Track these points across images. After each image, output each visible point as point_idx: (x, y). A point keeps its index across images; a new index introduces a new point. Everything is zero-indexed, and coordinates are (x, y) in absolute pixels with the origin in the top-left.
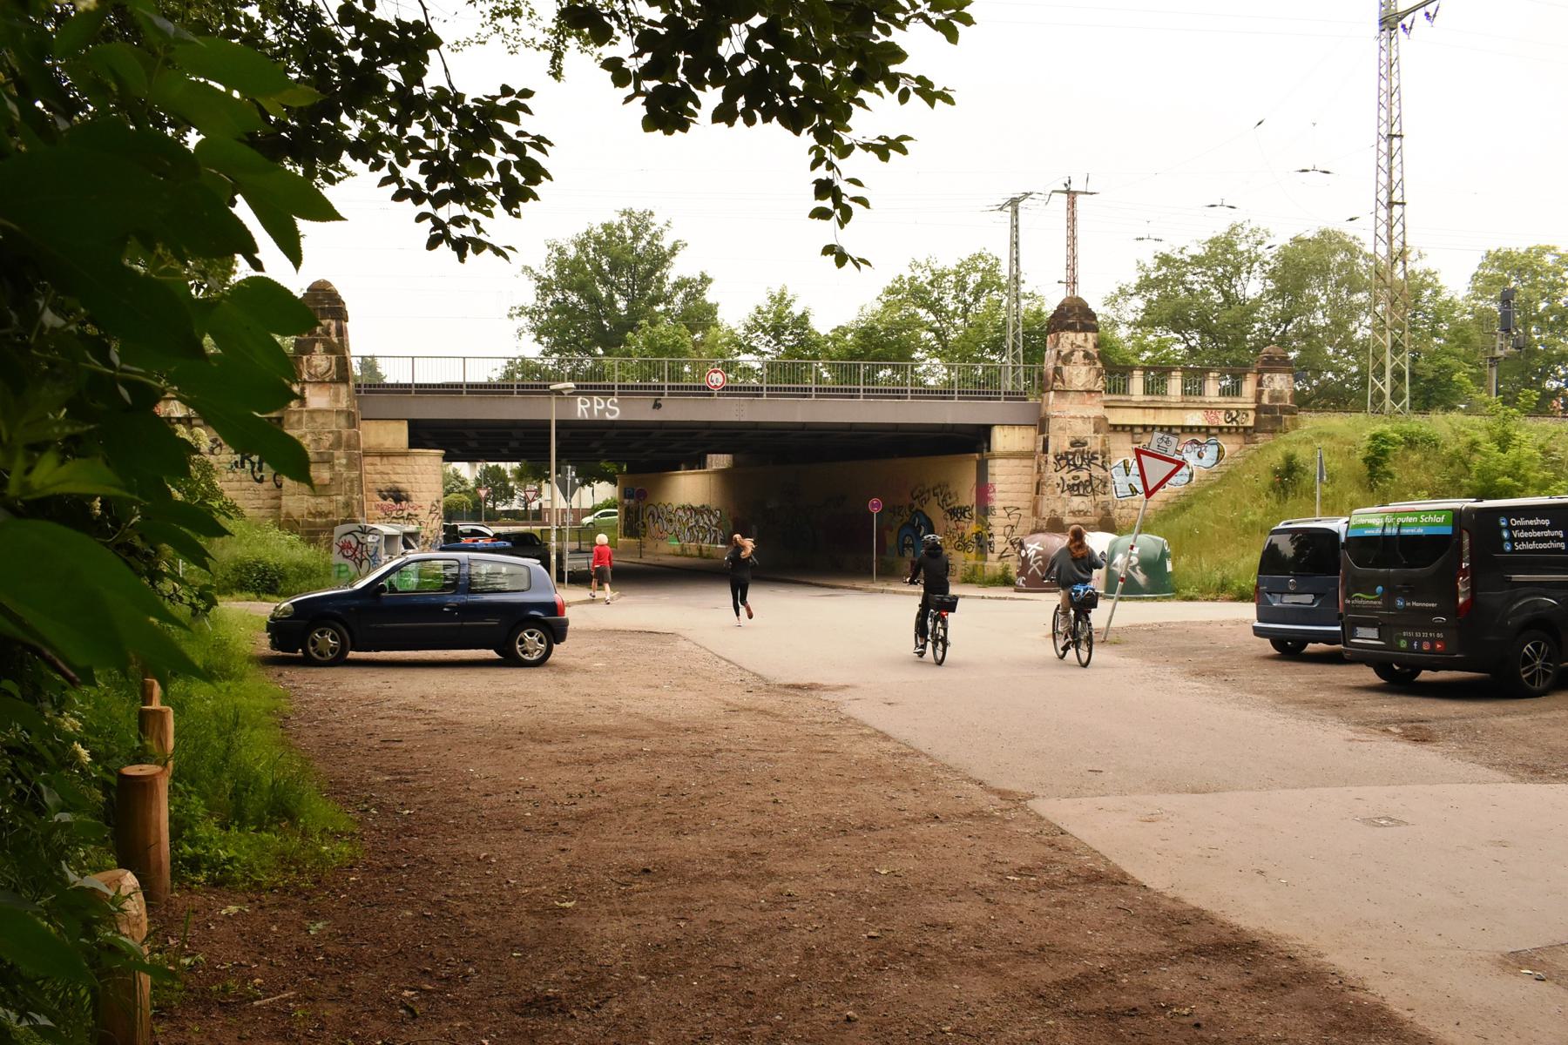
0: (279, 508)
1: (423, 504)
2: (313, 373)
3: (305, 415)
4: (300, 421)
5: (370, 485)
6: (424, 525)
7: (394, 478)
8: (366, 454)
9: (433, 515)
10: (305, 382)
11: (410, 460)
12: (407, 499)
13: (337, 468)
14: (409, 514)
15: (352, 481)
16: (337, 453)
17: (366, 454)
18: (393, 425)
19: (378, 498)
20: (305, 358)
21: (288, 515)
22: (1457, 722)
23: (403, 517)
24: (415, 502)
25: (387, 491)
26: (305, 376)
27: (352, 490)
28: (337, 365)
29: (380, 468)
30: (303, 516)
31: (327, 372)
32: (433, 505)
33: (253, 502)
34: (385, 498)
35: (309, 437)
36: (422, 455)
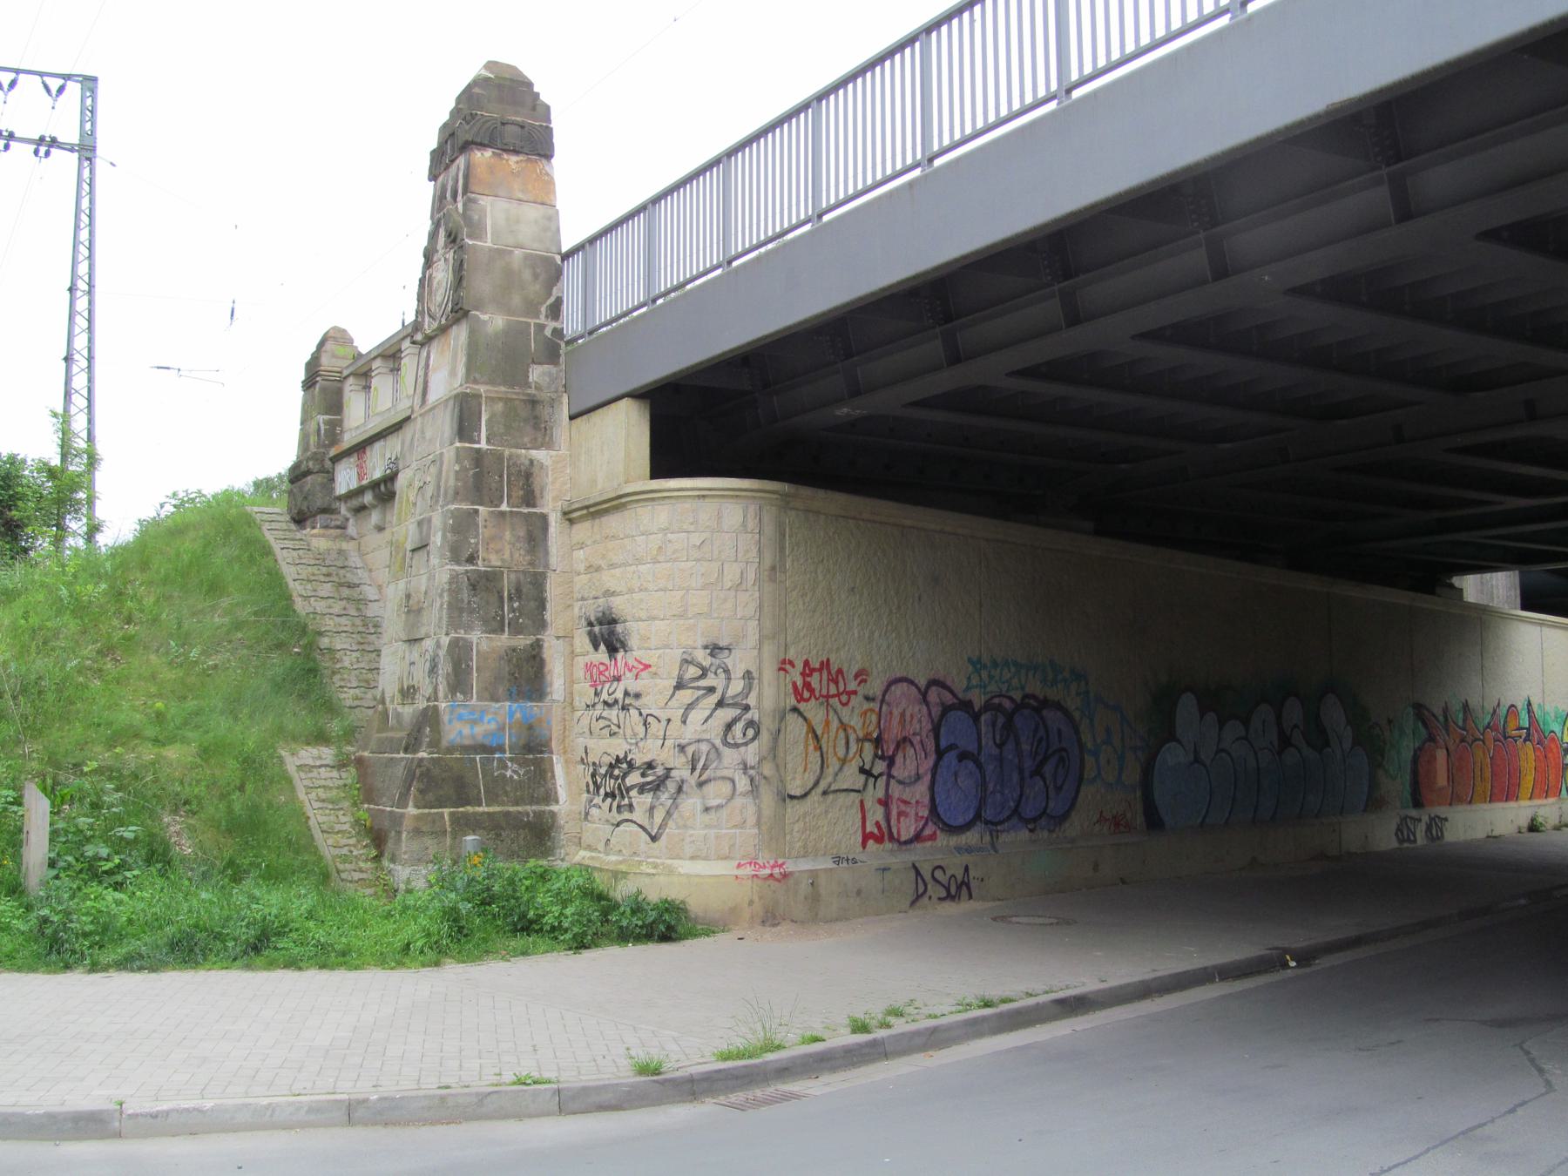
9: (686, 696)
32: (688, 661)
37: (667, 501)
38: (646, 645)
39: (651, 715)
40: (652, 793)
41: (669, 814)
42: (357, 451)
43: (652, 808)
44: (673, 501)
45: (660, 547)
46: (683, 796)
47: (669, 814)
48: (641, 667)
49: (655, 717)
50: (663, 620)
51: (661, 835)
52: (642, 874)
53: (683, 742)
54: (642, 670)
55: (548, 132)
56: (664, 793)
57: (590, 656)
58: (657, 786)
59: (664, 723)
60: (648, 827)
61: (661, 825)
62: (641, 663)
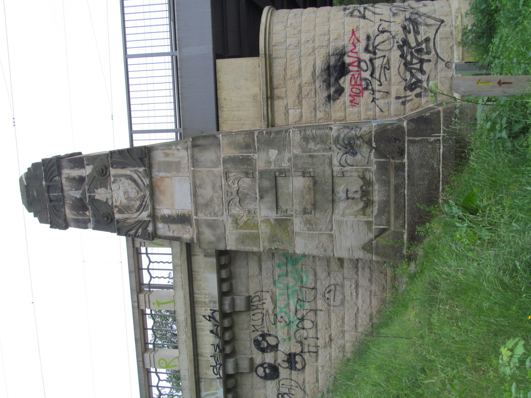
0: (356, 263)
1: (349, 29)
2: (138, 203)
3: (202, 216)
4: (211, 225)
5: (320, 115)
6: (385, 25)
7: (306, 76)
8: (271, 123)
10: (153, 217)
11: (278, 52)
12: (341, 54)
13: (285, 165)
14: (367, 50)
15: (306, 139)
16: (260, 165)
17: (271, 123)
18: (224, 79)
19: (339, 103)
20: (117, 216)
21: (367, 247)
22: (360, 320)
23: (371, 60)
24: (346, 41)
25: (329, 86)
26: (144, 215)
27: (323, 140)
28: (123, 166)
29: (291, 99)
30: (369, 223)
31: (134, 181)
33: (347, 292)
34: (340, 91)
35: (236, 210)
36: (269, 33)
37: (271, 26)
38: (342, 35)
39: (378, 28)
40: (419, 26)
41: (429, 17)
42: (191, 256)
43: (427, 25)
44: (272, 24)
45: (294, 28)
46: (419, 13)
47: (429, 17)
48: (354, 36)
49: (379, 27)
50: (330, 27)
51: (440, 19)
52: (462, 21)
53: (391, 14)
54: (355, 36)
55: (45, 162)
56: (418, 21)
57: (346, 100)
58: (415, 23)
59: (382, 22)
60: (437, 27)
61: (435, 20)
62: (352, 37)
